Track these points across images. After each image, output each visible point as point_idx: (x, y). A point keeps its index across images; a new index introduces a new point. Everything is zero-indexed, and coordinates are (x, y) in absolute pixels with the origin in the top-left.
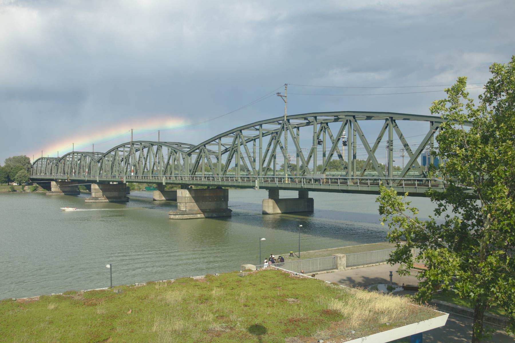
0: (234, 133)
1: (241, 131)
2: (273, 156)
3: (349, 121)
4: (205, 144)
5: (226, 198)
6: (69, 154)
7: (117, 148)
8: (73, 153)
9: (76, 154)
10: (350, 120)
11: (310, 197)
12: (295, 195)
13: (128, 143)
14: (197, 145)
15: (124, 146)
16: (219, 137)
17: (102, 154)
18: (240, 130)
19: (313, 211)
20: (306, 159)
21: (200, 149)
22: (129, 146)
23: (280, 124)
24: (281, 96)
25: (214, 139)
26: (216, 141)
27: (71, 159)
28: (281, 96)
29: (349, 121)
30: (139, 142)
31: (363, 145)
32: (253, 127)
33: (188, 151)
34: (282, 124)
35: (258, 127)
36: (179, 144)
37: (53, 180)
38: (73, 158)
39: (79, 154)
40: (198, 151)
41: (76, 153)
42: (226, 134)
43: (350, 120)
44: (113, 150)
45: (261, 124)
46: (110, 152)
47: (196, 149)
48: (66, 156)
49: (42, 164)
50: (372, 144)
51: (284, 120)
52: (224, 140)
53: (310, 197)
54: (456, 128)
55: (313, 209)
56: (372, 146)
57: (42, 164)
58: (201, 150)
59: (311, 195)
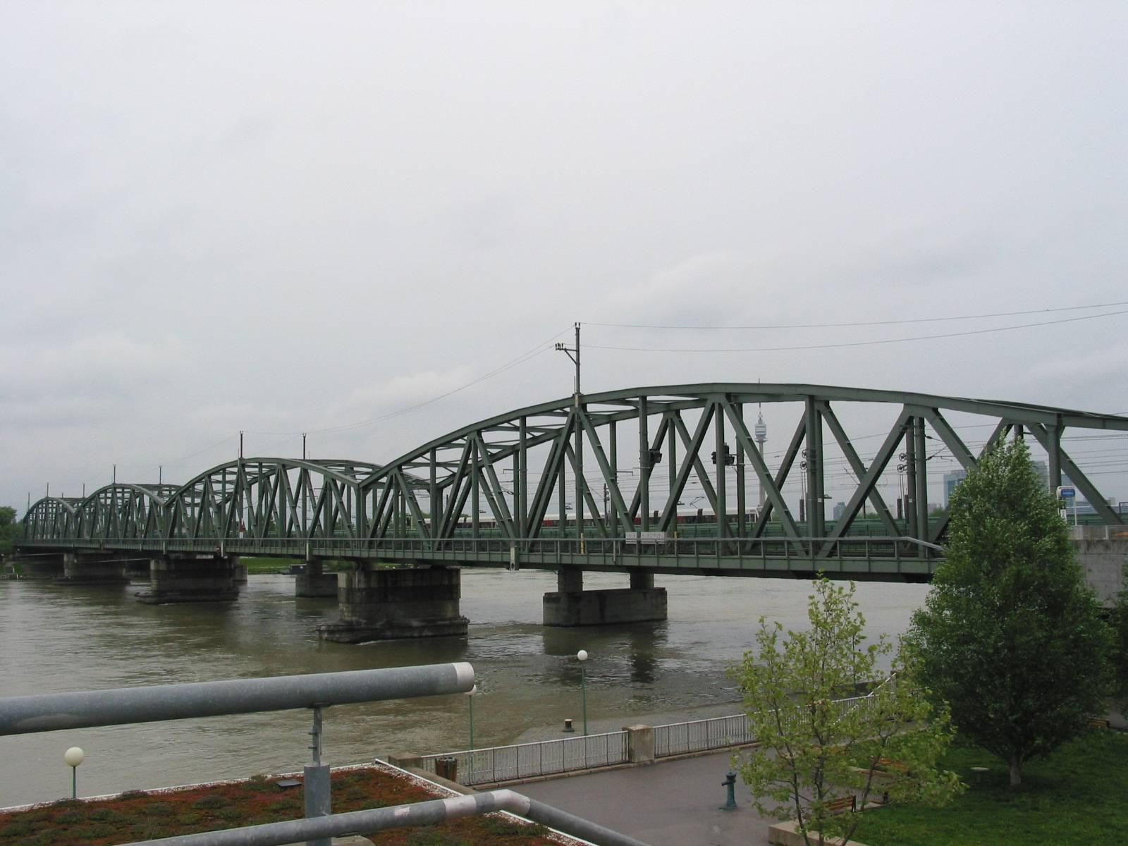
0: (466, 438)
1: (479, 433)
2: (650, 458)
3: (717, 406)
4: (400, 464)
5: (452, 592)
6: (104, 490)
7: (208, 474)
8: (114, 487)
9: (120, 490)
10: (719, 404)
11: (656, 585)
12: (621, 581)
13: (233, 465)
14: (385, 465)
15: (224, 470)
16: (432, 448)
17: (177, 488)
18: (478, 429)
19: (666, 619)
20: (693, 471)
21: (390, 474)
22: (235, 470)
23: (565, 414)
24: (566, 350)
25: (419, 452)
26: (425, 456)
27: (109, 502)
28: (566, 350)
29: (717, 406)
30: (256, 461)
31: (704, 490)
32: (508, 422)
33: (363, 481)
34: (571, 415)
35: (517, 423)
36: (349, 466)
37: (68, 550)
38: (113, 499)
39: (126, 490)
40: (384, 480)
41: (119, 488)
42: (447, 442)
43: (719, 404)
44: (198, 480)
45: (522, 414)
46: (192, 484)
47: (382, 477)
48: (98, 493)
49: (46, 513)
50: (774, 468)
51: (574, 405)
52: (443, 455)
53: (656, 585)
54: (883, 670)
55: (666, 614)
56: (774, 474)
57: (46, 513)
58: (392, 477)
59: (659, 581)
